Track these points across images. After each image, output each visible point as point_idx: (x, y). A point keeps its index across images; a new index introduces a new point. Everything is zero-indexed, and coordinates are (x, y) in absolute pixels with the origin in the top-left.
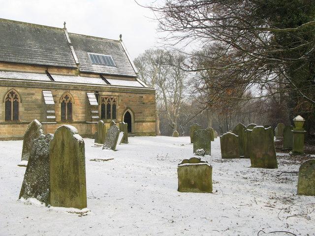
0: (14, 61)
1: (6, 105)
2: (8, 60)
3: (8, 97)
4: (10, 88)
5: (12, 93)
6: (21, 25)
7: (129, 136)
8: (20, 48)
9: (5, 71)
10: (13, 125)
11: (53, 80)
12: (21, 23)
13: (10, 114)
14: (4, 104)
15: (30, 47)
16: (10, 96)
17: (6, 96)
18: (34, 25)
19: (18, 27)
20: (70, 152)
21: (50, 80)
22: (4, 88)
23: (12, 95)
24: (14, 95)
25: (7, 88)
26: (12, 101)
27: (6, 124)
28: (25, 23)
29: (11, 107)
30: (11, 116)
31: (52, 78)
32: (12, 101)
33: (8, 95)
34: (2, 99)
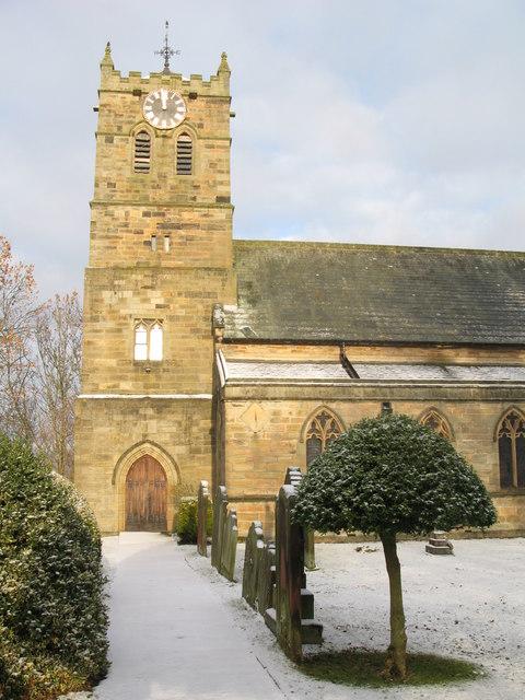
0: (491, 340)
1: (500, 447)
2: (480, 340)
3: (504, 429)
4: (507, 405)
5: (512, 418)
6: (484, 258)
7: (321, 540)
8: (497, 308)
9: (476, 366)
10: (519, 498)
11: (357, 376)
12: (482, 252)
13: (510, 470)
14: (497, 444)
15: (517, 305)
16: (509, 426)
17: (500, 427)
18: (509, 253)
19: (478, 262)
20: (105, 623)
21: (348, 377)
22: (494, 405)
23: (512, 423)
24: (517, 422)
25: (499, 406)
26: (324, 439)
27: (503, 496)
28: (492, 253)
29: (510, 452)
30: (512, 477)
31: (355, 373)
32: (324, 439)
33: (313, 424)
34: (490, 434)
